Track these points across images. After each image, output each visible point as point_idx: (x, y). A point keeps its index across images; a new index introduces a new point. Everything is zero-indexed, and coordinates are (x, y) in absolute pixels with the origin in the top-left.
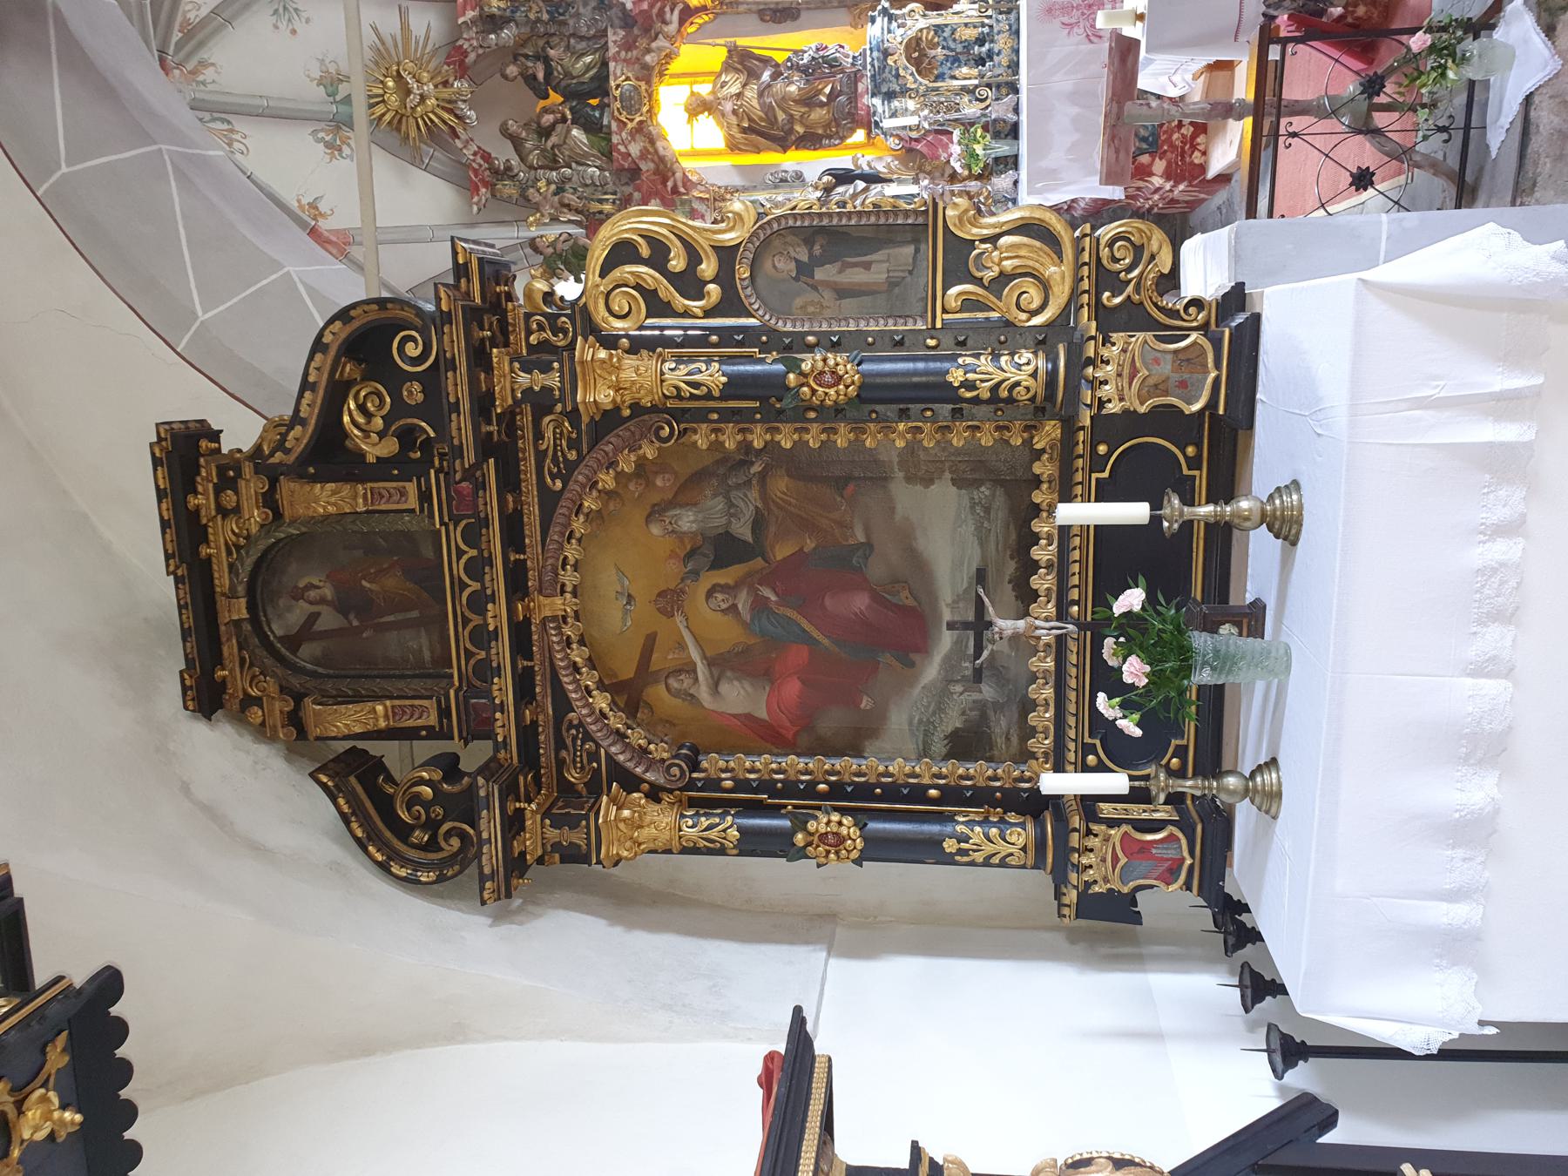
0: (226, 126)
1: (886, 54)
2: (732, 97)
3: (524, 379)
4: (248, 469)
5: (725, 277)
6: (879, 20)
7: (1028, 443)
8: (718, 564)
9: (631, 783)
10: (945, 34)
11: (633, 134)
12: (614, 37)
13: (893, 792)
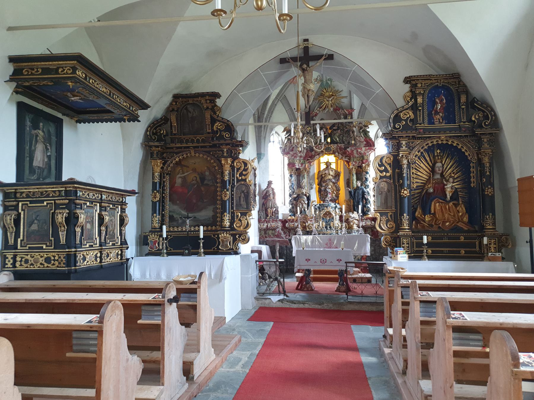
1: (327, 207)
3: (225, 150)
4: (213, 105)
5: (242, 180)
6: (335, 205)
7: (218, 225)
8: (200, 178)
9: (164, 164)
12: (342, 145)
13: (163, 206)
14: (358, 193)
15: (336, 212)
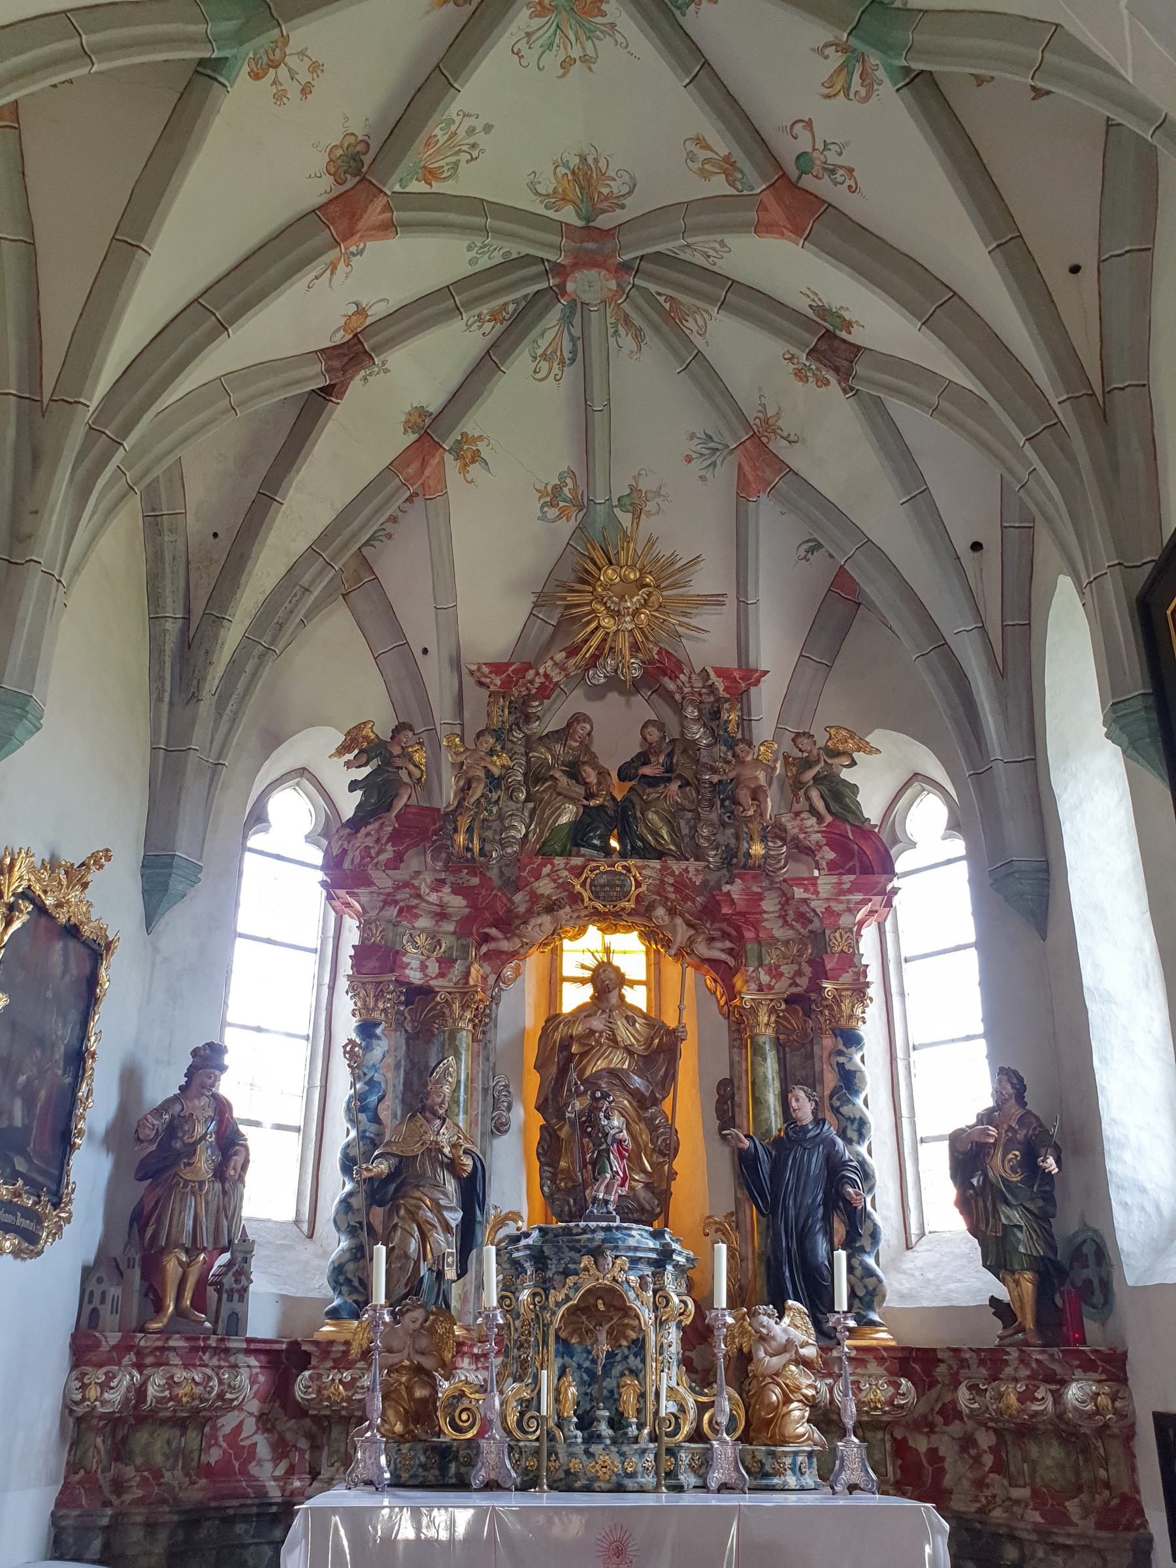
0: (567, 355)
2: (612, 1030)
10: (631, 1358)
11: (566, 886)
14: (800, 1170)
15: (661, 1300)
